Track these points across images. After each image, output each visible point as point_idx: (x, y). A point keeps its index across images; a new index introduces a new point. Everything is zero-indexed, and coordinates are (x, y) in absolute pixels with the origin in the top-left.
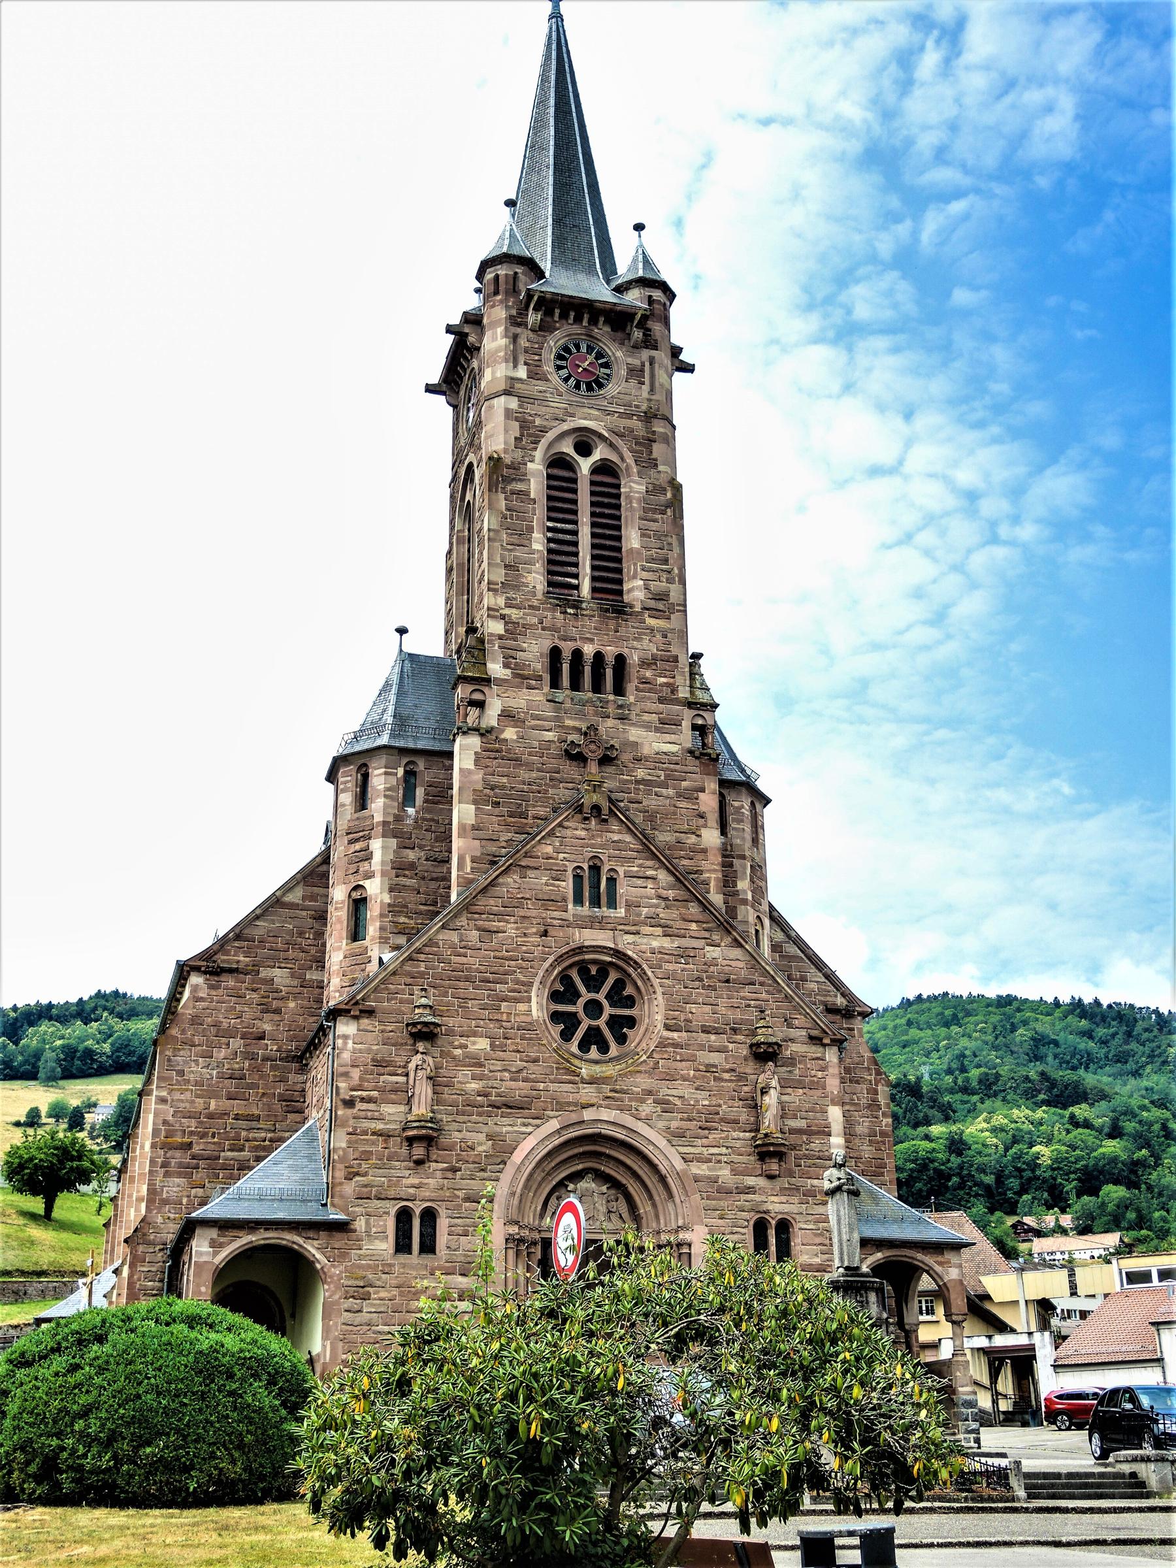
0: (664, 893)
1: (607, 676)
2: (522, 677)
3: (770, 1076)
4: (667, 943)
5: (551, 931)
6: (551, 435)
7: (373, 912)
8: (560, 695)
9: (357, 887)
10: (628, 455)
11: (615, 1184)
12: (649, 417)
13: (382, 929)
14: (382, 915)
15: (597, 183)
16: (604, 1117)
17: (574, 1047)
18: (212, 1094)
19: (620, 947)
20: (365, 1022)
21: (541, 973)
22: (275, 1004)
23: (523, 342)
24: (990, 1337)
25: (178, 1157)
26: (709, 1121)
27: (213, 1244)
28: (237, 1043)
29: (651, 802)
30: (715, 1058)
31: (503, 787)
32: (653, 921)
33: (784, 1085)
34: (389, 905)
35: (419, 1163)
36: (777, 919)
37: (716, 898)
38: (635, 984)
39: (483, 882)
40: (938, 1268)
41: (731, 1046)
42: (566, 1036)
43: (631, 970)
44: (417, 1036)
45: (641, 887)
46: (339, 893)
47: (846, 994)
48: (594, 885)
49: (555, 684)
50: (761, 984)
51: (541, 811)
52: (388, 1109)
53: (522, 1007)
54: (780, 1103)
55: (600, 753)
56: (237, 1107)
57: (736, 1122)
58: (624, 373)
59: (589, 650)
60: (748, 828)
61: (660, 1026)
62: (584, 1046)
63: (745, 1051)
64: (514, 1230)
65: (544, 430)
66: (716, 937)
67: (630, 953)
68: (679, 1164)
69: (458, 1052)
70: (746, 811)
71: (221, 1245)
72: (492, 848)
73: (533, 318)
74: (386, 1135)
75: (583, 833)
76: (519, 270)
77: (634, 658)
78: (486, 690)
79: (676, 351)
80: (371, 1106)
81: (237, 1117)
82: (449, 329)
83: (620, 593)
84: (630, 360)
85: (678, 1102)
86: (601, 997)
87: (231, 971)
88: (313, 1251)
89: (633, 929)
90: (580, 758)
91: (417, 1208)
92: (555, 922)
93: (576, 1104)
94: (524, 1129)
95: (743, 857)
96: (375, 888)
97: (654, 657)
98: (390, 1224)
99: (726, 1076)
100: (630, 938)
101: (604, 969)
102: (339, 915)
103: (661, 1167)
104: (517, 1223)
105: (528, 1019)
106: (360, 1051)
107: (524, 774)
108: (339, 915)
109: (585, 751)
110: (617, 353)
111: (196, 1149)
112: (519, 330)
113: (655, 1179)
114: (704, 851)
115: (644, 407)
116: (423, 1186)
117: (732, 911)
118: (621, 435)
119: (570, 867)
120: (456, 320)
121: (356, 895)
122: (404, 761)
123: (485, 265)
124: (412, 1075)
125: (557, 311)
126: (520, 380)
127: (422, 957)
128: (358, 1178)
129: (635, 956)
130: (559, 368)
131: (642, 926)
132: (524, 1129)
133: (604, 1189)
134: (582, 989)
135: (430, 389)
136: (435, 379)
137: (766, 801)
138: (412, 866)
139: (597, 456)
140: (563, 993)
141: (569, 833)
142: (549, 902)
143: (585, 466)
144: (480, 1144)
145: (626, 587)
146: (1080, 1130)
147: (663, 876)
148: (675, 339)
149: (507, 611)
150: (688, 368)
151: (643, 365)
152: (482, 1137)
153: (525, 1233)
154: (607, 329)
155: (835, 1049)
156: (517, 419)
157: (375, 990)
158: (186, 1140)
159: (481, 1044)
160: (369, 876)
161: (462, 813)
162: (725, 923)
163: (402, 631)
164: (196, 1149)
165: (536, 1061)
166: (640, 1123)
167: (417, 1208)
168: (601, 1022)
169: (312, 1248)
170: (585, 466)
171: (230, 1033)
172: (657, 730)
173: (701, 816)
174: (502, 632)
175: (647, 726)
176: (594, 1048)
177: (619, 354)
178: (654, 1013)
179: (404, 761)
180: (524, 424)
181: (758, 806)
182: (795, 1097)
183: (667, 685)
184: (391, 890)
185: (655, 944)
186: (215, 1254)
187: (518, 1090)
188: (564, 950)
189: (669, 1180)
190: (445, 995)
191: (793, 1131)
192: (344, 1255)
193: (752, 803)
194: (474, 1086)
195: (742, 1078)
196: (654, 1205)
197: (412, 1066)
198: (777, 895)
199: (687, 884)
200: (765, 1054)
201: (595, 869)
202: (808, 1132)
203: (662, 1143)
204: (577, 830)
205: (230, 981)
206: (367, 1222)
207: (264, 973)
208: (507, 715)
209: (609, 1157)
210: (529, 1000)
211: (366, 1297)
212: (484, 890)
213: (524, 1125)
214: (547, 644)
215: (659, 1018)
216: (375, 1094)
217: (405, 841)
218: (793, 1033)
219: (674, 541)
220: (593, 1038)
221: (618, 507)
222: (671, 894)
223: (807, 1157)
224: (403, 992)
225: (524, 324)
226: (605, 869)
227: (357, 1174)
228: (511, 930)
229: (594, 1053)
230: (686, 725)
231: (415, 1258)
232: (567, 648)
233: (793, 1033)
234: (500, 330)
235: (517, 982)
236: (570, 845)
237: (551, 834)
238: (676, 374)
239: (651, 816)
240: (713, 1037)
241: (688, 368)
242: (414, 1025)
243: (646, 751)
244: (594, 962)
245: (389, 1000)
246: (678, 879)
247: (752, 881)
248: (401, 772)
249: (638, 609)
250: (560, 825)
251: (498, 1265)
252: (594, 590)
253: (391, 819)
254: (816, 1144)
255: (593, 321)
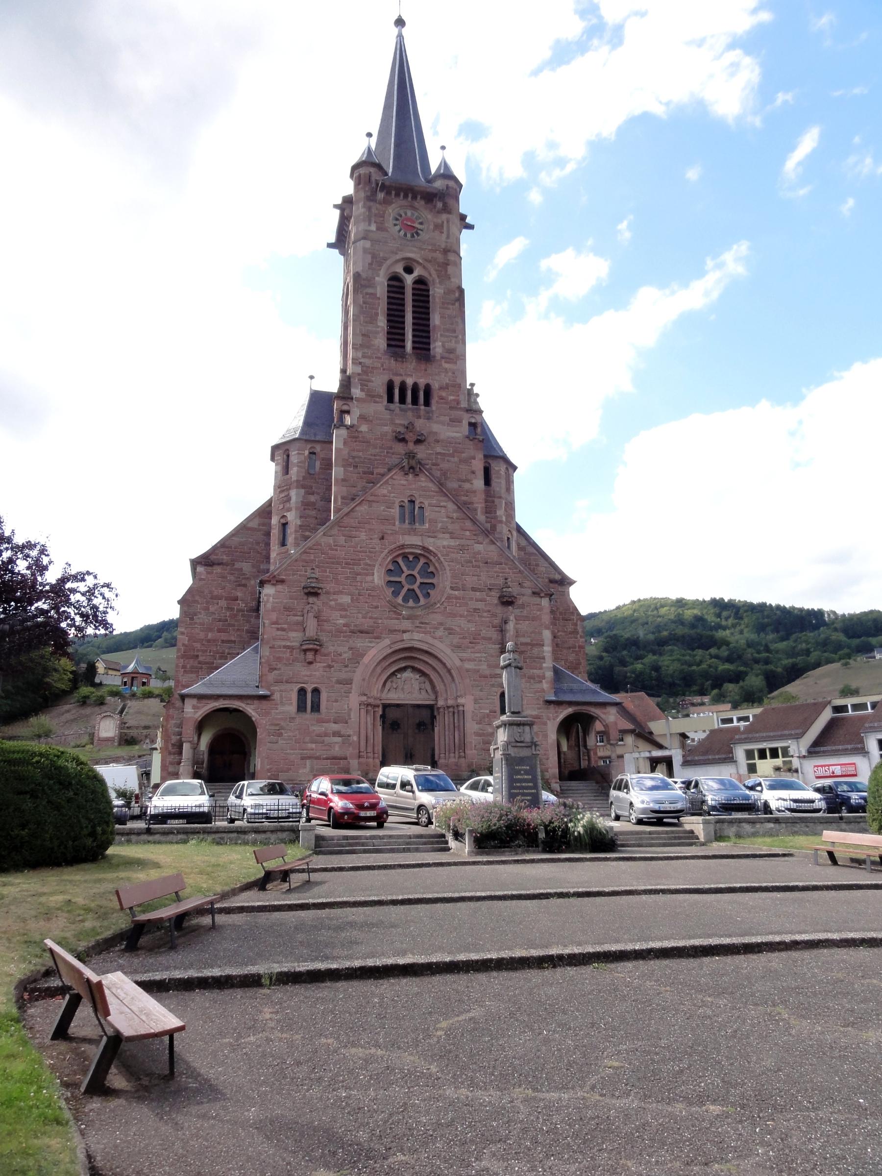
0: (451, 515)
1: (422, 396)
2: (371, 396)
3: (512, 613)
4: (453, 543)
5: (386, 536)
6: (389, 262)
7: (290, 530)
8: (392, 406)
9: (284, 516)
10: (434, 273)
11: (423, 674)
12: (446, 251)
13: (296, 539)
14: (296, 531)
15: (762, 608)
16: (415, 638)
17: (400, 600)
18: (210, 630)
19: (426, 545)
20: (280, 587)
21: (380, 559)
22: (244, 582)
23: (374, 210)
24: (650, 752)
25: (191, 662)
26: (475, 639)
27: (194, 707)
28: (223, 603)
29: (444, 466)
30: (480, 605)
31: (359, 457)
32: (445, 530)
33: (517, 618)
34: (300, 526)
35: (310, 663)
36: (519, 529)
37: (481, 517)
38: (434, 565)
39: (346, 510)
40: (603, 716)
41: (488, 598)
42: (396, 594)
43: (432, 558)
44: (309, 594)
45: (439, 512)
46: (275, 520)
47: (560, 572)
48: (412, 512)
49: (390, 400)
50: (506, 564)
51: (382, 471)
52: (293, 634)
53: (369, 578)
54: (515, 628)
55: (415, 438)
56: (223, 636)
57: (490, 639)
58: (432, 227)
59: (410, 382)
60: (503, 482)
61: (448, 588)
62: (406, 600)
63: (496, 601)
64: (364, 698)
65: (385, 259)
66: (480, 539)
67: (431, 548)
68: (458, 663)
69: (333, 603)
70: (503, 472)
71: (198, 708)
72: (353, 491)
73: (381, 196)
74: (292, 648)
75: (404, 482)
76: (372, 170)
77: (435, 386)
78: (350, 404)
79: (463, 217)
80: (283, 633)
81: (223, 641)
82: (336, 206)
83: (429, 350)
84: (435, 220)
85: (457, 629)
86: (415, 573)
87: (219, 564)
88: (251, 711)
89: (432, 535)
90: (403, 440)
91: (309, 688)
92: (389, 532)
93: (399, 631)
94: (369, 645)
95: (500, 497)
96: (291, 516)
97: (447, 385)
98: (294, 696)
99: (485, 614)
100: (432, 540)
101: (417, 557)
102: (275, 533)
103: (448, 665)
104: (365, 695)
105: (372, 585)
106: (277, 603)
107: (372, 451)
108: (275, 533)
109: (407, 437)
110: (428, 215)
111: (201, 659)
112: (372, 204)
113: (445, 671)
114: (475, 492)
115: (443, 247)
116: (313, 675)
117: (494, 528)
118: (430, 261)
119: (397, 501)
120: (339, 201)
121: (283, 521)
122: (309, 446)
123: (355, 168)
124: (305, 616)
125: (393, 192)
126: (372, 231)
127: (312, 551)
128: (276, 672)
129: (434, 550)
130: (395, 225)
131: (441, 535)
132: (369, 645)
133: (417, 677)
134: (404, 568)
135: (330, 245)
136: (333, 239)
137: (515, 468)
138: (314, 504)
139: (416, 274)
140: (394, 570)
141: (396, 482)
142: (386, 520)
143: (409, 279)
144: (345, 652)
145: (432, 347)
146: (713, 660)
147: (451, 506)
148: (462, 210)
149: (362, 360)
150: (470, 227)
151: (443, 222)
152: (346, 649)
153: (371, 701)
154: (423, 202)
155: (547, 599)
156: (370, 253)
157: (286, 570)
158: (196, 653)
159: (346, 599)
160: (289, 510)
161: (336, 472)
162: (489, 532)
163: (312, 377)
164: (201, 659)
165: (377, 607)
166: (436, 641)
167: (309, 688)
168: (415, 587)
169: (250, 709)
170: (409, 279)
171: (219, 598)
172: (448, 424)
173: (473, 472)
174: (360, 371)
175: (443, 423)
176: (411, 601)
177: (429, 217)
178: (444, 581)
179: (309, 446)
180: (374, 256)
181: (510, 470)
182: (524, 626)
183: (454, 400)
184: (301, 517)
185: (445, 543)
186: (195, 713)
187: (367, 624)
188: (393, 546)
189: (452, 671)
190: (326, 571)
191: (522, 644)
192: (267, 713)
193: (507, 469)
194: (342, 621)
195: (494, 615)
196: (445, 685)
197: (305, 611)
198: (522, 517)
199: (465, 508)
200: (507, 602)
201: (412, 502)
202: (533, 645)
203: (448, 651)
204: (399, 479)
205: (218, 570)
206: (281, 696)
207: (238, 565)
208: (362, 418)
209: (427, 663)
210: (373, 574)
211: (280, 735)
212: (347, 514)
213: (370, 642)
214: (385, 379)
215: (448, 584)
216: (285, 626)
217: (309, 492)
218: (523, 591)
219: (460, 321)
220: (412, 594)
221: (428, 302)
222: (455, 515)
223: (531, 658)
224: (301, 571)
225: (374, 201)
226: (417, 503)
227: (275, 669)
228: (363, 536)
229: (411, 603)
230: (465, 423)
231: (308, 715)
232: (397, 381)
233: (523, 591)
234: (361, 204)
235: (367, 564)
236: (397, 488)
237: (386, 482)
238: (464, 231)
239: (444, 473)
240: (478, 593)
241: (470, 227)
242: (307, 588)
243: (442, 437)
244: (412, 553)
245: (293, 575)
246: (459, 507)
247: (506, 510)
248: (307, 453)
249: (438, 357)
250: (391, 478)
251: (354, 716)
252: (414, 348)
253: (301, 479)
254: (536, 651)
255: (414, 198)
